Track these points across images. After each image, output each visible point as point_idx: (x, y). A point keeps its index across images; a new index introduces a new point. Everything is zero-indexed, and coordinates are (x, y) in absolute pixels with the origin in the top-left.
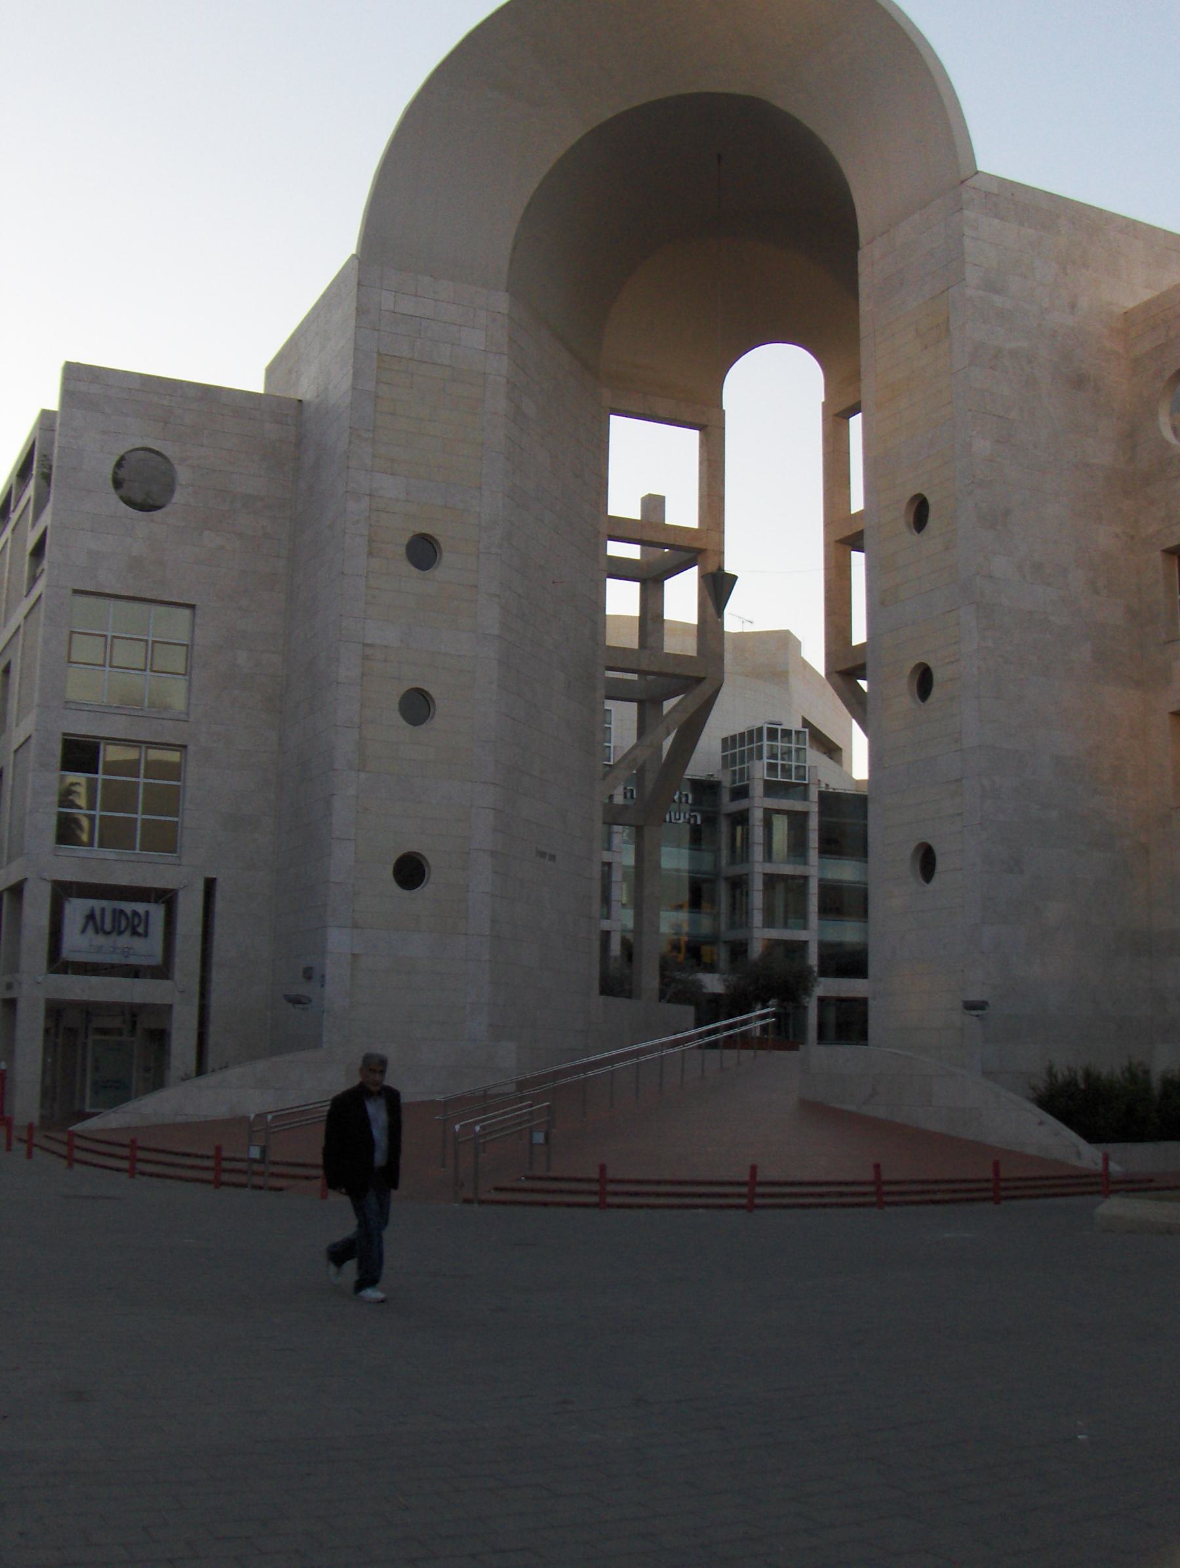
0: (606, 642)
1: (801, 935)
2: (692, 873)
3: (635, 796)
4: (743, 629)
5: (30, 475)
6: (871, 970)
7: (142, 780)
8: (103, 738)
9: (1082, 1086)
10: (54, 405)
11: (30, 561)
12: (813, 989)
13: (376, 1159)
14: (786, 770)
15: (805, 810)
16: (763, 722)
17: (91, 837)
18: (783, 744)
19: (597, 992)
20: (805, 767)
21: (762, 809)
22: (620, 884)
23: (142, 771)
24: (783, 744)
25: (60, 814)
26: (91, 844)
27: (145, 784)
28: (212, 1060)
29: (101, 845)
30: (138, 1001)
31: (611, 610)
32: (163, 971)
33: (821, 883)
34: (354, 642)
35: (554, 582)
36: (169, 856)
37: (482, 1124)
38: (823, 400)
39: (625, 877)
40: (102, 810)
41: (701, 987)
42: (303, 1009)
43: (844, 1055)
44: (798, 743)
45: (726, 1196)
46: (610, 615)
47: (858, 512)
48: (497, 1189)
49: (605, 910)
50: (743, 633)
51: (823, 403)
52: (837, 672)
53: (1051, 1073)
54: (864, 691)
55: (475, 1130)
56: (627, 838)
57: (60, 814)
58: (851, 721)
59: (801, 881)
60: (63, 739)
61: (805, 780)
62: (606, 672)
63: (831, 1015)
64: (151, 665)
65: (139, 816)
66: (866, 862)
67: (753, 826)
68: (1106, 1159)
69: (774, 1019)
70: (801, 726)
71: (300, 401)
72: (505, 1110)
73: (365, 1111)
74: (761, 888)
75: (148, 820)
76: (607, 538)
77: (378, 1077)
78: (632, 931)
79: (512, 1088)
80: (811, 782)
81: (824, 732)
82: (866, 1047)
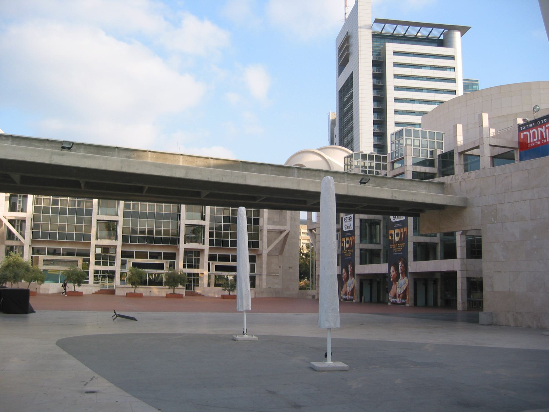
1: (367, 169)
4: (461, 136)
6: (394, 67)
7: (215, 231)
8: (329, 148)
10: (481, 87)
11: (281, 240)
14: (226, 235)
15: (301, 290)
18: (195, 257)
20: (435, 141)
22: (432, 233)
23: (78, 216)
24: (195, 257)
25: (237, 223)
26: (234, 269)
27: (50, 207)
28: (395, 100)
30: (413, 302)
33: (467, 239)
34: (18, 285)
37: (398, 211)
38: (5, 193)
40: (221, 238)
41: (165, 281)
45: (419, 66)
46: (311, 213)
47: (489, 123)
48: (336, 135)
49: (261, 282)
56: (529, 145)
57: (237, 223)
58: (4, 132)
59: (236, 214)
62: (458, 309)
63: (64, 226)
64: (416, 139)
70: (412, 178)
71: (43, 260)
73: (251, 309)
74: (457, 236)
76: (299, 223)
79: (94, 292)
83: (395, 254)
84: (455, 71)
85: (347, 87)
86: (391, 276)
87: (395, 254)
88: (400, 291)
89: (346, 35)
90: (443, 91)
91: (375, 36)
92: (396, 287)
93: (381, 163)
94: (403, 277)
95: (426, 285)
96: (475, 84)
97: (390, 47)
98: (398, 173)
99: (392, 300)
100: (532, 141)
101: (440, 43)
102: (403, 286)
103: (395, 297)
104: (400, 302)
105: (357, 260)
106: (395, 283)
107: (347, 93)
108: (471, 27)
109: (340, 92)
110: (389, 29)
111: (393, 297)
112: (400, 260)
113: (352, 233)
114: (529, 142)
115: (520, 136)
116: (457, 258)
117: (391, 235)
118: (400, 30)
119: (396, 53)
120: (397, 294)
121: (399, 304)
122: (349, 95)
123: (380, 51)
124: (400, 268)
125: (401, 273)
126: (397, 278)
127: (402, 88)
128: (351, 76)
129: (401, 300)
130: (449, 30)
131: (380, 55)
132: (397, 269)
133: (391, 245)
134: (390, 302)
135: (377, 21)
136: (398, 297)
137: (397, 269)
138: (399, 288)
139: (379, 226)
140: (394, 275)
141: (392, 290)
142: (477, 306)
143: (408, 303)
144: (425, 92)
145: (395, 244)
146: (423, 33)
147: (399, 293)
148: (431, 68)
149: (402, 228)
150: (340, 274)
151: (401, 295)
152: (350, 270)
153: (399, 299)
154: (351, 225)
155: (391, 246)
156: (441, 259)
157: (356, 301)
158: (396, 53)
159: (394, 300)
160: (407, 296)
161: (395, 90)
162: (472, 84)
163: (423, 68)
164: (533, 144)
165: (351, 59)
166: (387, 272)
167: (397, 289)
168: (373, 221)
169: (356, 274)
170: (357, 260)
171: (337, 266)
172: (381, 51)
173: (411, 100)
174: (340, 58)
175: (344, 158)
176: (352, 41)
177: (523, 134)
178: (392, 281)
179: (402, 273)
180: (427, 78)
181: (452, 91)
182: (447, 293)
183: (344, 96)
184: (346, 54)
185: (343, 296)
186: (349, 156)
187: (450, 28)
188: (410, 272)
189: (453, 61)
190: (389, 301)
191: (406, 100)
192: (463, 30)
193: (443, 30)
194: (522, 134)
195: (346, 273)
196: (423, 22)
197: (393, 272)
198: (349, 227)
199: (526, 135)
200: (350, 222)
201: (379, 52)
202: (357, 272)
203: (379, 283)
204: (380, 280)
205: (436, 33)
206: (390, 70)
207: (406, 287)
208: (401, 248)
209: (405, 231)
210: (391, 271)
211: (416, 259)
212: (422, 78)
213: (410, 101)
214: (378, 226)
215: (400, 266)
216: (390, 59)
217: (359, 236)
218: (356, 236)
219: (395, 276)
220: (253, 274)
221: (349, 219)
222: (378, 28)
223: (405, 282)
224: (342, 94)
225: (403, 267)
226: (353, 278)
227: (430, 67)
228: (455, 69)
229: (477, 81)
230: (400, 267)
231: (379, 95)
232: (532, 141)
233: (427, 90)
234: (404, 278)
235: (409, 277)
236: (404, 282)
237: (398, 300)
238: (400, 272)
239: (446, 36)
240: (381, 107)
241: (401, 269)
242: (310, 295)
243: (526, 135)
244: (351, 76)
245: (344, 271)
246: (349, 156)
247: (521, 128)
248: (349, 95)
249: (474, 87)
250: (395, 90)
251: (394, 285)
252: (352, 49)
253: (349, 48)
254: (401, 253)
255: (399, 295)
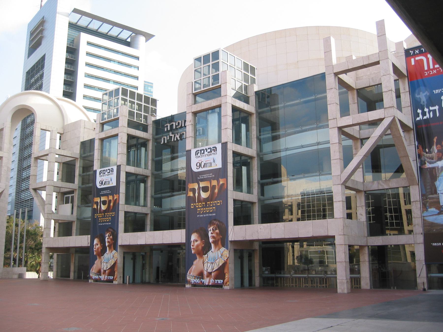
0: (361, 182)
2: (277, 278)
3: (283, 279)
5: (219, 181)
9: (283, 207)
12: (22, 246)
13: (333, 62)
16: (90, 130)
17: (322, 283)
19: (379, 65)
21: (385, 107)
29: (349, 249)
31: (288, 243)
32: (203, 155)
35: (95, 129)
36: (210, 288)
39: (75, 205)
42: (342, 229)
43: (411, 236)
44: (292, 284)
45: (109, 60)
50: (405, 55)
51: (440, 161)
52: (32, 189)
53: (302, 145)
54: (432, 112)
55: (108, 142)
60: (351, 278)
61: (435, 110)
62: (339, 291)
63: (326, 212)
65: (371, 215)
66: (69, 22)
67: (320, 180)
68: (44, 253)
69: (373, 201)
72: (368, 170)
75: (323, 197)
77: (266, 268)
78: (206, 284)
80: (125, 166)
81: (238, 226)
82: (332, 188)
83: (101, 224)
84: (138, 70)
85: (36, 68)
86: (94, 249)
87: (101, 224)
88: (106, 266)
89: (41, 20)
90: (127, 85)
91: (72, 26)
92: (101, 262)
93: (150, 106)
94: (217, 248)
95: (134, 259)
96: (150, 85)
97: (85, 38)
98: (208, 107)
99: (94, 277)
100: (431, 67)
101: (128, 44)
102: (218, 260)
103: (99, 273)
104: (105, 280)
105: (121, 226)
106: (100, 257)
107: (36, 74)
108: (154, 36)
109: (28, 73)
110: (84, 22)
111: (95, 274)
112: (108, 231)
113: (115, 190)
114: (426, 68)
115: (408, 63)
116: (335, 216)
117: (193, 190)
118: (95, 25)
119: (89, 43)
120: (102, 270)
121: (104, 281)
122: (38, 75)
123: (74, 39)
124: (106, 240)
125: (109, 246)
126: (206, 248)
127: (92, 76)
128: (43, 58)
129: (106, 276)
130: (136, 34)
131: (73, 43)
132: (102, 241)
133: (192, 204)
134: (92, 279)
135: (76, 11)
136: (207, 277)
137: (102, 241)
138: (209, 264)
139: (143, 184)
140: (98, 249)
141: (95, 266)
142: (296, 286)
143: (228, 285)
144: (111, 83)
145: (199, 201)
146: (115, 32)
147: (105, 269)
148: (119, 63)
149: (214, 180)
150: (89, 245)
151: (107, 272)
152: (109, 240)
153: (104, 275)
154: (111, 180)
155: (192, 206)
156: (151, 231)
157: (118, 282)
158: (89, 43)
159: (97, 277)
160: (116, 272)
161: (85, 76)
162: (148, 85)
163: (112, 61)
164: (435, 71)
165: (44, 42)
166: (184, 241)
167: (102, 264)
168: (139, 177)
169: (120, 246)
170: (121, 226)
171: (71, 237)
172: (75, 40)
173: (99, 89)
174: (31, 42)
175: (103, 94)
176: (47, 26)
177: (415, 59)
178: (194, 255)
179: (109, 246)
180: (114, 71)
181: (134, 87)
182: (264, 268)
183: (32, 76)
184: (39, 37)
185: (93, 276)
186: (113, 90)
187: (137, 32)
188: (233, 240)
189: (137, 61)
190: (91, 278)
191: (95, 88)
192: (148, 36)
193: (132, 33)
194: (413, 60)
195: (101, 244)
196: (117, 22)
197: (97, 245)
198: (107, 183)
199: (422, 60)
200: (110, 176)
201: (73, 41)
202: (120, 242)
203: (143, 257)
204: (146, 253)
205: (125, 35)
206: (83, 59)
207: (114, 262)
208: (215, 208)
209: (223, 184)
210: (95, 243)
211: (126, 230)
212: (110, 70)
213: (98, 89)
214: (142, 185)
215: (106, 238)
216: (83, 49)
217: (124, 194)
218: (120, 194)
219: (100, 250)
220: (349, 211)
221: (110, 172)
222: (75, 18)
223: (113, 257)
224: (30, 75)
225: (111, 239)
226: (114, 251)
227: (118, 62)
228: (138, 68)
229: (152, 84)
230: (108, 239)
231: (69, 79)
232: (431, 67)
233: (114, 82)
234: (112, 252)
235: (118, 251)
236: (112, 257)
237: (103, 277)
238: (107, 244)
239: (133, 38)
240: (70, 91)
241: (109, 242)
242: (16, 274)
243: (422, 60)
244: (43, 58)
245: (96, 241)
246: (113, 90)
247: (410, 52)
248: (38, 75)
249: (149, 88)
250: (85, 76)
251: (98, 260)
252: (46, 33)
253: (43, 32)
254: (110, 223)
255: (105, 271)
